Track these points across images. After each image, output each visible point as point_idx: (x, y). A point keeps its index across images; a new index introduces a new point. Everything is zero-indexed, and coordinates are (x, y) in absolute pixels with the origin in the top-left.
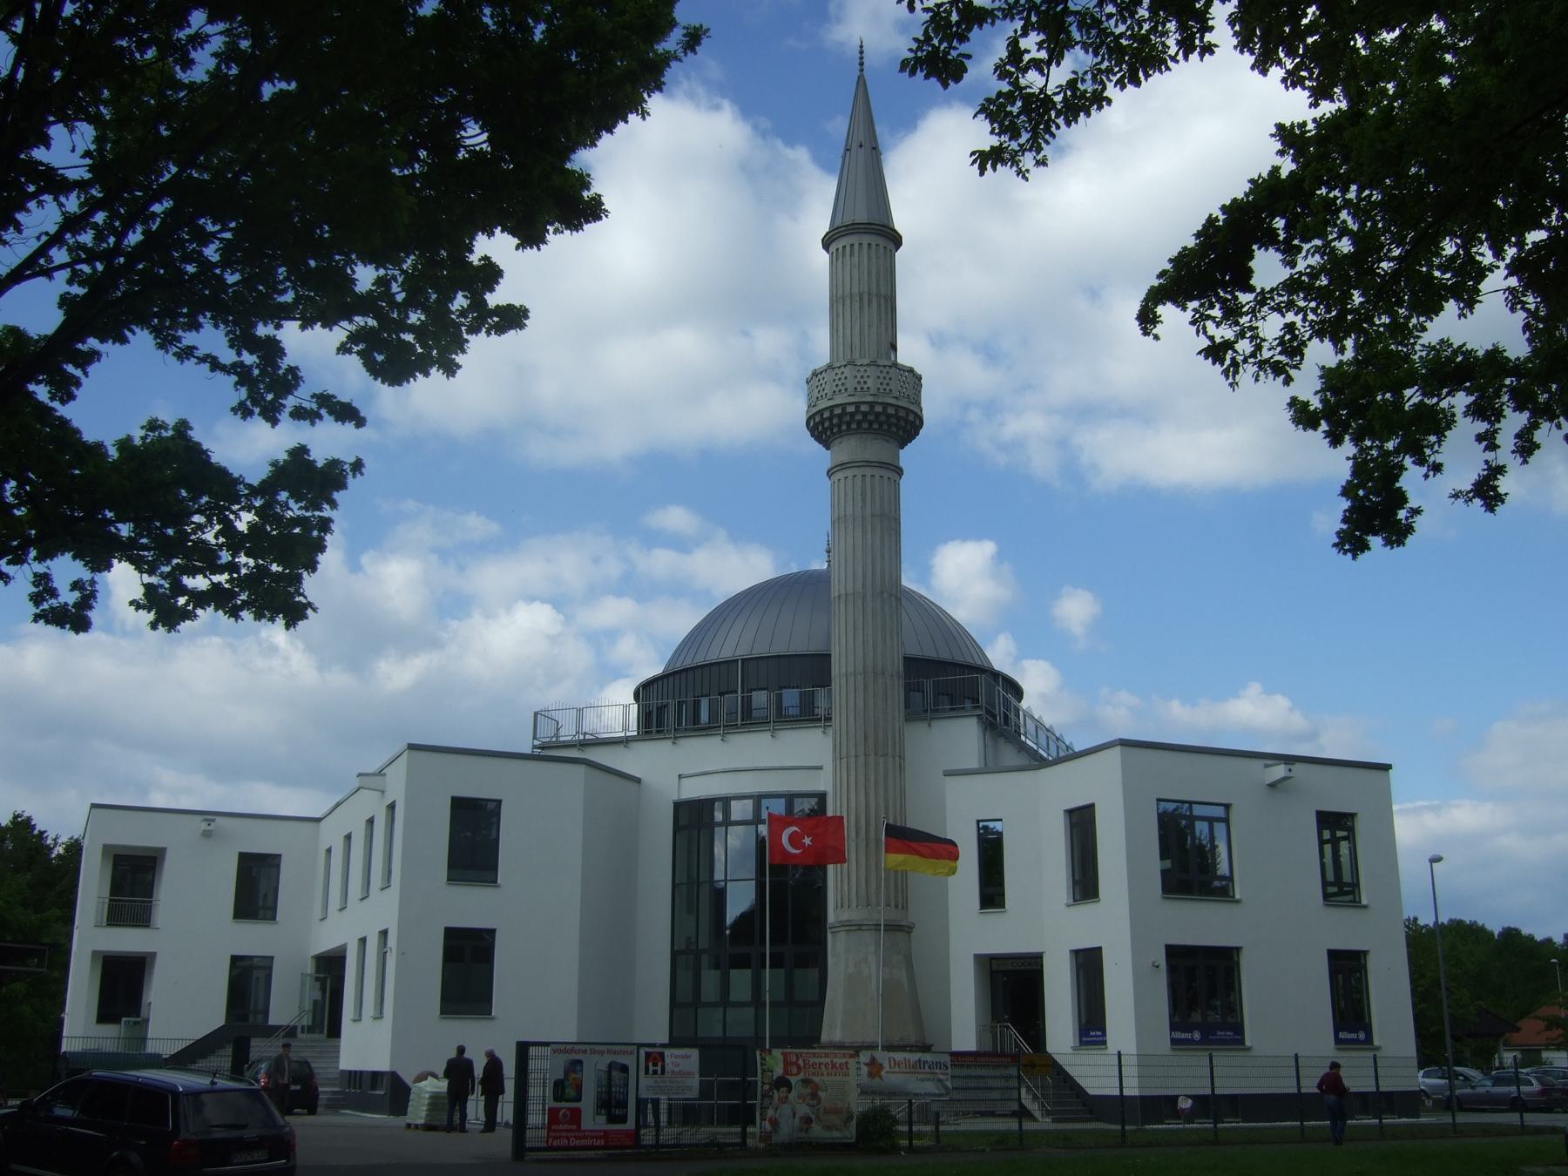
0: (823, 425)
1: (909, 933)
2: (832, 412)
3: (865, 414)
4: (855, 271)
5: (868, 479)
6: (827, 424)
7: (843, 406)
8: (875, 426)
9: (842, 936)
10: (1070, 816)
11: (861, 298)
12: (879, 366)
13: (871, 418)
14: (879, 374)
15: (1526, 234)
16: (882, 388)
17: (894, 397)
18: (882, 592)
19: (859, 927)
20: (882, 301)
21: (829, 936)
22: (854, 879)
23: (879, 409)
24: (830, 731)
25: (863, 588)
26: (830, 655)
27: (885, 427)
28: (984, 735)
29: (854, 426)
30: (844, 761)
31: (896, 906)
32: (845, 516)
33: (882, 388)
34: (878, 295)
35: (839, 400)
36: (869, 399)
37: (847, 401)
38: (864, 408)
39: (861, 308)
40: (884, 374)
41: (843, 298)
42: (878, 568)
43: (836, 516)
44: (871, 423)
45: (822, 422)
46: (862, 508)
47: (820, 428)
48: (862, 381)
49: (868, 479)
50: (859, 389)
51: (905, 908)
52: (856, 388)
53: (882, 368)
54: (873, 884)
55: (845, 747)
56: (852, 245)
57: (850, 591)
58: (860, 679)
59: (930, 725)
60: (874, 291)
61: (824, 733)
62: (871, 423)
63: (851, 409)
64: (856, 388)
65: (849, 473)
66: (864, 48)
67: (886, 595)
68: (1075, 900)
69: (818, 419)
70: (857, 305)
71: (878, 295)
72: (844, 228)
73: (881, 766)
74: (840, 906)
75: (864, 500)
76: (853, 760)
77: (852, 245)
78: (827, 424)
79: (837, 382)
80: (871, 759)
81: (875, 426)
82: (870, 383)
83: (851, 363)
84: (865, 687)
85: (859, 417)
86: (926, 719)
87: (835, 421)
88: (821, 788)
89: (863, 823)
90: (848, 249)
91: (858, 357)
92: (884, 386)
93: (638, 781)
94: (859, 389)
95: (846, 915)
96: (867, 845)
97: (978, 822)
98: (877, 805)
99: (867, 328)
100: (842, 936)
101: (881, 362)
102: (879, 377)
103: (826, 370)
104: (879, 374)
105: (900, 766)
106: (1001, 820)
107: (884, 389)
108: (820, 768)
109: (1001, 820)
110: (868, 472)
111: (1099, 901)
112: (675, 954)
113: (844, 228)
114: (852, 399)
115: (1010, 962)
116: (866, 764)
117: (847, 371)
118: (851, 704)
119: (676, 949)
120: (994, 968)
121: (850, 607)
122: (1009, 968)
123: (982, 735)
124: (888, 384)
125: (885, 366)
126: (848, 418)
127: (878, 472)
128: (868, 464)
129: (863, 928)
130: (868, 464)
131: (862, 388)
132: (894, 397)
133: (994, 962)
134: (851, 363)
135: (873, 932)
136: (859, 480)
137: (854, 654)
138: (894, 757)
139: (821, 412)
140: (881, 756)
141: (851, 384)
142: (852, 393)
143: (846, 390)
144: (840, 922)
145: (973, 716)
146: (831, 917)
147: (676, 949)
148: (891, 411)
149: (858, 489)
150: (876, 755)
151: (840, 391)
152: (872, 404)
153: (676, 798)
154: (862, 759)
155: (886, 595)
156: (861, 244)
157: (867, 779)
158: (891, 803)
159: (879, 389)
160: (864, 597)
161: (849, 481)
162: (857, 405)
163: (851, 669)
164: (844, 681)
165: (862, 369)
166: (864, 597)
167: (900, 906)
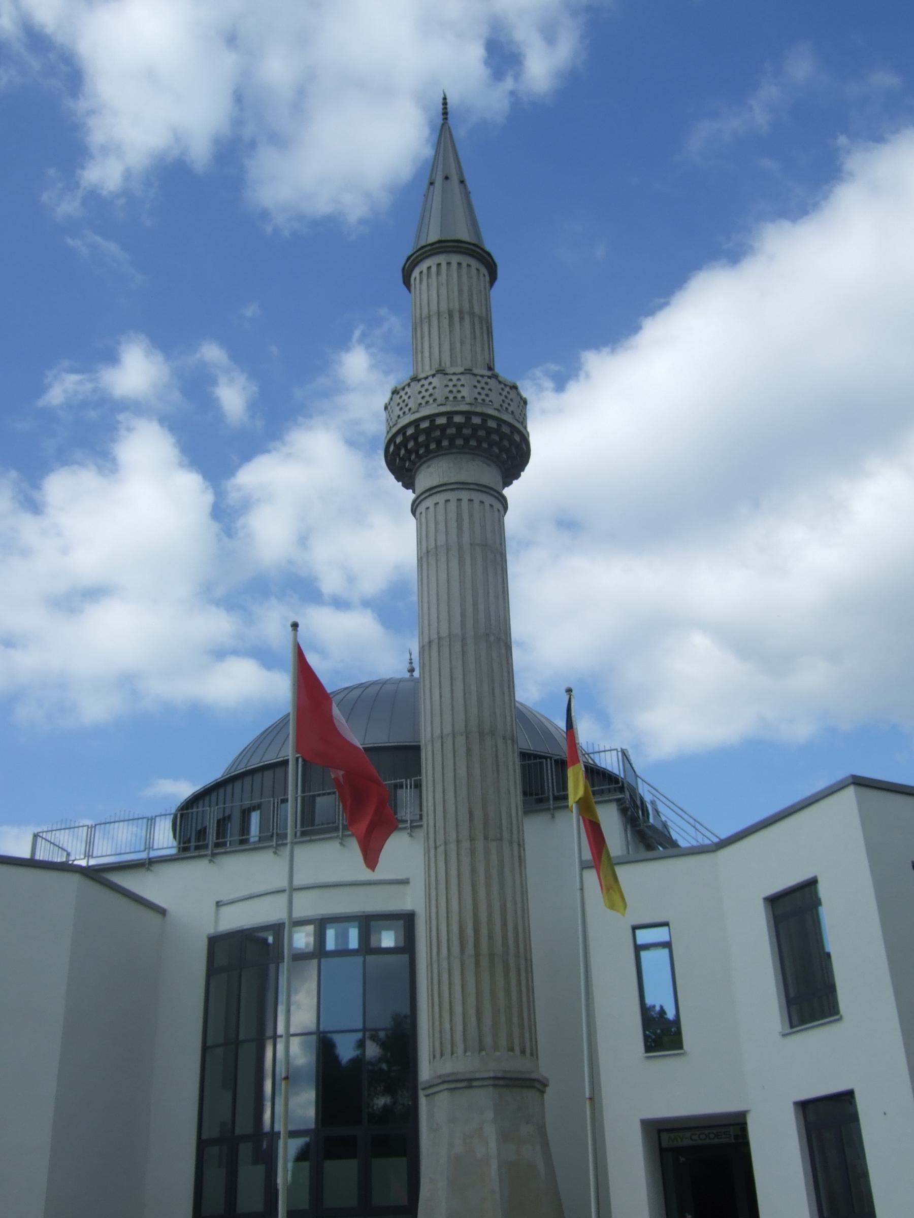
0: (406, 447)
1: (542, 1092)
2: (417, 426)
3: (459, 427)
4: (444, 291)
5: (465, 504)
6: (411, 445)
7: (431, 418)
8: (473, 443)
9: (443, 1099)
10: (772, 908)
11: (451, 315)
12: (475, 375)
13: (466, 431)
14: (476, 384)
15: (666, 1016)
16: (480, 398)
17: (495, 409)
18: (488, 635)
19: (469, 1083)
20: (477, 320)
21: (423, 1101)
22: (458, 1009)
23: (476, 420)
24: (420, 834)
25: (462, 629)
26: (417, 749)
27: (485, 445)
28: (626, 826)
29: (445, 443)
30: (441, 850)
31: (523, 1052)
32: (436, 547)
33: (480, 398)
34: (472, 314)
35: (425, 412)
36: (464, 408)
37: (436, 411)
38: (458, 419)
39: (451, 324)
40: (483, 385)
41: (429, 317)
42: (481, 607)
43: (424, 550)
44: (466, 439)
45: (404, 443)
46: (458, 536)
47: (403, 452)
48: (455, 390)
49: (465, 504)
50: (451, 398)
51: (534, 1054)
52: (447, 398)
53: (479, 378)
54: (488, 1020)
55: (442, 832)
56: (439, 265)
57: (444, 632)
58: (461, 740)
59: (553, 817)
60: (466, 307)
61: (411, 836)
62: (466, 439)
63: (442, 421)
64: (447, 398)
65: (440, 498)
66: (448, 106)
67: (492, 638)
68: (792, 1026)
69: (399, 440)
70: (446, 322)
71: (472, 314)
72: (429, 248)
73: (494, 857)
74: (439, 1054)
75: (460, 528)
76: (453, 846)
77: (439, 265)
78: (411, 445)
79: (424, 393)
80: (480, 844)
81: (473, 443)
82: (465, 392)
83: (441, 371)
84: (469, 750)
85: (451, 431)
86: (549, 809)
87: (421, 439)
88: (407, 905)
89: (470, 932)
90: (434, 269)
91: (448, 364)
92: (483, 397)
93: (162, 912)
94: (451, 398)
95: (448, 1067)
96: (477, 963)
97: (635, 928)
98: (489, 906)
99: (458, 345)
100: (443, 1099)
101: (475, 371)
102: (475, 387)
103: (409, 385)
104: (476, 384)
105: (520, 857)
106: (666, 924)
107: (483, 400)
108: (406, 882)
109: (666, 924)
110: (465, 495)
111: (840, 1019)
112: (202, 1145)
113: (429, 248)
114: (443, 409)
115: (688, 1134)
116: (473, 852)
117: (435, 381)
118: (450, 775)
119: (204, 1137)
120: (665, 1144)
121: (445, 654)
122: (687, 1142)
123: (623, 833)
124: (487, 395)
125: (482, 376)
126: (438, 433)
127: (477, 497)
128: (463, 486)
129: (475, 1084)
130: (463, 486)
131: (455, 398)
132: (495, 409)
133: (665, 1136)
134: (441, 371)
135: (491, 1089)
136: (453, 505)
137: (453, 710)
138: (511, 843)
139: (403, 430)
140: (494, 840)
141: (440, 395)
142: (443, 403)
143: (435, 400)
144: (440, 1077)
145: (610, 801)
146: (425, 1072)
147: (204, 1137)
148: (492, 424)
149: (453, 515)
150: (486, 838)
151: (427, 402)
152: (468, 415)
153: (211, 931)
154: (466, 845)
155: (492, 638)
156: (449, 264)
157: (473, 871)
158: (509, 905)
159: (476, 399)
160: (464, 640)
161: (441, 506)
162: (450, 415)
163: (448, 729)
164: (438, 745)
165: (455, 378)
166: (464, 640)
167: (528, 1052)
